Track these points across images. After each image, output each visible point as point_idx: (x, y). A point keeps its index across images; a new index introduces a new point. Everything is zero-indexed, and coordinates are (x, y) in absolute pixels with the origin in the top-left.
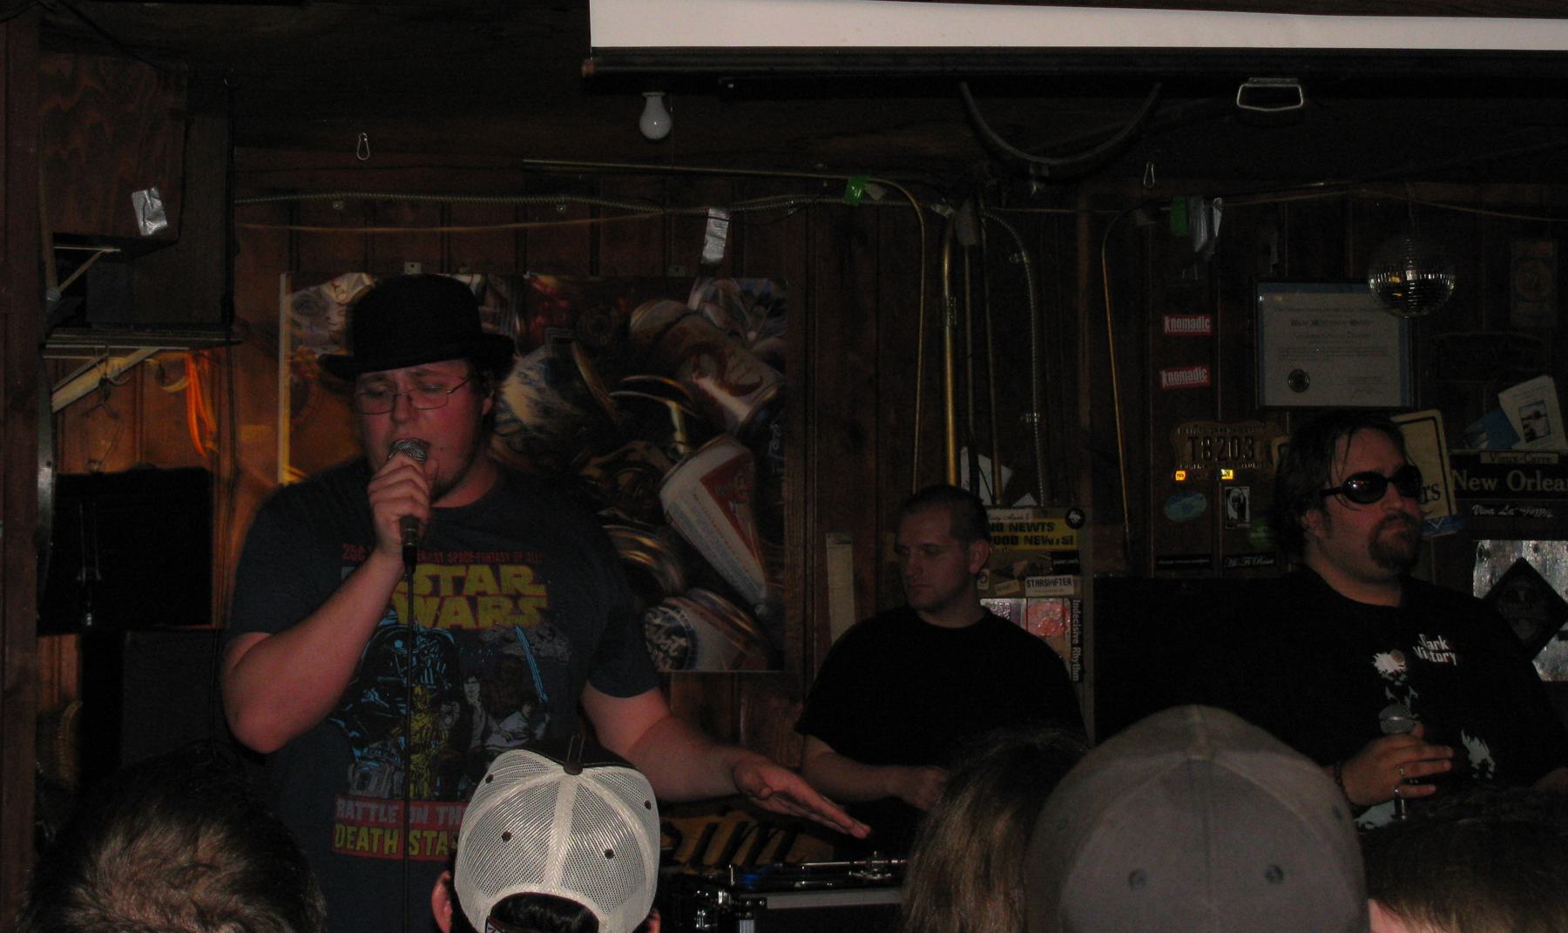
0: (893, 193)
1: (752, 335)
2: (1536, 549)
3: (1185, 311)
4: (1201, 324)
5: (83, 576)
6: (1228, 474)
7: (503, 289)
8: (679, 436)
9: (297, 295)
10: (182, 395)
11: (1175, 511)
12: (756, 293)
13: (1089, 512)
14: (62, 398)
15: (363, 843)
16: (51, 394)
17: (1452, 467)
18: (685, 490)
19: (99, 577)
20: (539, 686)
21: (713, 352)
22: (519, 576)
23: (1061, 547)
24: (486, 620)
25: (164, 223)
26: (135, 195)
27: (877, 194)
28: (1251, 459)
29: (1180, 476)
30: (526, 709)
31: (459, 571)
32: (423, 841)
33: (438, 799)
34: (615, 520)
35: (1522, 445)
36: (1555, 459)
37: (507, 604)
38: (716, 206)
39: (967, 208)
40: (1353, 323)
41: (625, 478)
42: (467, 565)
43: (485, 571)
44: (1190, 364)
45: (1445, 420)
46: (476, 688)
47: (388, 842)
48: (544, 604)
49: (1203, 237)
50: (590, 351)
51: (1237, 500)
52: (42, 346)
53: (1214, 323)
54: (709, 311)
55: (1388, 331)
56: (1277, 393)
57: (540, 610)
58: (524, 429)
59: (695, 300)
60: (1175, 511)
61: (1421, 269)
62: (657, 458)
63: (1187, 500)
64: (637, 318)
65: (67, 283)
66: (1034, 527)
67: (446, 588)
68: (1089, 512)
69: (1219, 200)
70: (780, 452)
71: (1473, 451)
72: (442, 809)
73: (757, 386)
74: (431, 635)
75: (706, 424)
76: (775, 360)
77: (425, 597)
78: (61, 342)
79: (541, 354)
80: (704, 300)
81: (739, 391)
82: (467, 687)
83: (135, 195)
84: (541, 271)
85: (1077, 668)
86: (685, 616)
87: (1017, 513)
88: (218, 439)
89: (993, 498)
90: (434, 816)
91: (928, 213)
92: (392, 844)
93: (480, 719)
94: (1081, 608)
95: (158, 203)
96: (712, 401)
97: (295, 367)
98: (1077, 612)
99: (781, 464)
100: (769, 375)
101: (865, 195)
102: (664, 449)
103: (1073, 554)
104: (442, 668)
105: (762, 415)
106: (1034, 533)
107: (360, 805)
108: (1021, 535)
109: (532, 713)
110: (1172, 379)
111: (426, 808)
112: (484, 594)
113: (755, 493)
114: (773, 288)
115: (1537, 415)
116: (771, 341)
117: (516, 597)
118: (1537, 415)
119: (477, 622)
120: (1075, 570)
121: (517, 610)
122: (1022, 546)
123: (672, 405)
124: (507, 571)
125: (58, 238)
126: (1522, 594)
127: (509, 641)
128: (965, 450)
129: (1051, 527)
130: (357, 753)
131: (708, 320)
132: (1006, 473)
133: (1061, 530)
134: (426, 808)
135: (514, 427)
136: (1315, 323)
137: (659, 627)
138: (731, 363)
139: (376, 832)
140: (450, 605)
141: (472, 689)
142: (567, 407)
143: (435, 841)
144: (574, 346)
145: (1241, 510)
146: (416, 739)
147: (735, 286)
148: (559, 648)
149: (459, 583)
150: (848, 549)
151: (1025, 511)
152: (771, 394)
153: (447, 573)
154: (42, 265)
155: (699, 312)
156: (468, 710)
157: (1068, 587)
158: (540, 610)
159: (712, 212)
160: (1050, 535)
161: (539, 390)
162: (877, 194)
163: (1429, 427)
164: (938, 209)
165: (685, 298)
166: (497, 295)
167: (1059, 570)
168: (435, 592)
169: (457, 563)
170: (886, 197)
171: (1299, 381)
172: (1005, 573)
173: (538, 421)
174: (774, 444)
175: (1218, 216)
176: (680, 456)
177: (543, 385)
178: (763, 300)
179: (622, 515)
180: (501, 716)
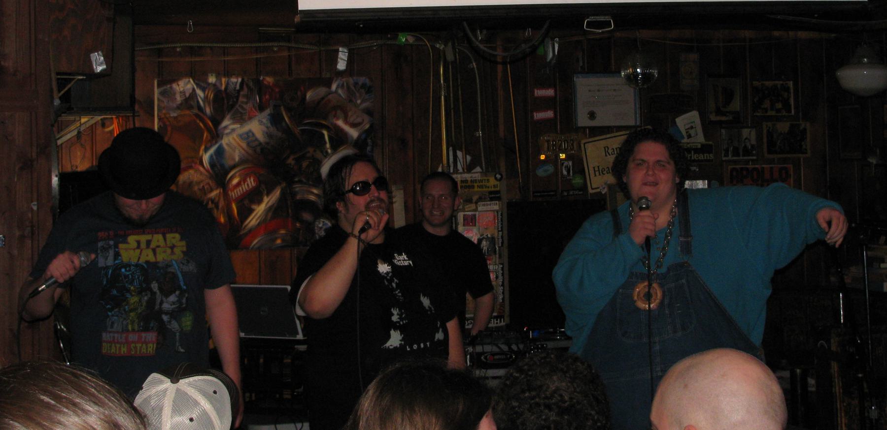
0: (418, 39)
1: (359, 102)
3: (543, 85)
4: (550, 92)
6: (563, 156)
7: (251, 84)
8: (328, 145)
9: (162, 89)
11: (541, 172)
12: (360, 83)
13: (504, 174)
15: (113, 350)
20: (182, 283)
21: (342, 109)
22: (174, 238)
23: (493, 189)
24: (160, 258)
25: (105, 67)
27: (411, 40)
28: (572, 150)
29: (543, 157)
30: (177, 293)
31: (149, 237)
32: (136, 348)
33: (142, 331)
34: (300, 182)
35: (685, 140)
36: (699, 146)
37: (169, 251)
38: (343, 46)
40: (615, 90)
41: (305, 164)
43: (160, 237)
44: (546, 109)
48: (185, 249)
49: (551, 55)
50: (289, 110)
51: (566, 167)
53: (556, 91)
54: (340, 91)
55: (629, 94)
56: (583, 120)
57: (183, 252)
58: (260, 144)
59: (334, 87)
60: (541, 172)
61: (642, 68)
62: (319, 155)
63: (546, 168)
64: (309, 95)
66: (481, 181)
67: (143, 245)
68: (504, 174)
70: (372, 151)
72: (143, 335)
74: (137, 265)
76: (369, 112)
79: (268, 111)
80: (337, 88)
81: (354, 125)
82: (152, 286)
85: (500, 241)
87: (474, 175)
91: (433, 47)
92: (124, 350)
95: (102, 58)
96: (342, 130)
97: (160, 119)
98: (500, 217)
100: (367, 118)
101: (406, 40)
102: (322, 152)
103: (498, 192)
105: (363, 136)
107: (112, 335)
108: (476, 185)
109: (180, 294)
110: (539, 116)
112: (158, 247)
114: (367, 81)
115: (692, 128)
116: (366, 105)
117: (173, 247)
118: (692, 128)
120: (499, 199)
121: (173, 253)
122: (476, 189)
124: (169, 236)
125: (58, 74)
127: (170, 266)
128: (451, 148)
130: (110, 314)
131: (340, 95)
132: (469, 158)
133: (492, 181)
135: (257, 143)
137: (321, 228)
138: (350, 114)
139: (118, 346)
141: (155, 286)
142: (280, 134)
145: (568, 172)
147: (351, 81)
148: (191, 267)
149: (148, 243)
150: (402, 192)
151: (476, 174)
152: (367, 126)
153: (143, 238)
155: (336, 92)
157: (495, 206)
158: (183, 252)
159: (340, 49)
161: (267, 127)
162: (411, 40)
164: (438, 46)
165: (329, 87)
166: (247, 85)
167: (492, 199)
168: (139, 247)
171: (592, 115)
173: (267, 140)
174: (369, 148)
177: (269, 125)
178: (364, 86)
180: (167, 296)
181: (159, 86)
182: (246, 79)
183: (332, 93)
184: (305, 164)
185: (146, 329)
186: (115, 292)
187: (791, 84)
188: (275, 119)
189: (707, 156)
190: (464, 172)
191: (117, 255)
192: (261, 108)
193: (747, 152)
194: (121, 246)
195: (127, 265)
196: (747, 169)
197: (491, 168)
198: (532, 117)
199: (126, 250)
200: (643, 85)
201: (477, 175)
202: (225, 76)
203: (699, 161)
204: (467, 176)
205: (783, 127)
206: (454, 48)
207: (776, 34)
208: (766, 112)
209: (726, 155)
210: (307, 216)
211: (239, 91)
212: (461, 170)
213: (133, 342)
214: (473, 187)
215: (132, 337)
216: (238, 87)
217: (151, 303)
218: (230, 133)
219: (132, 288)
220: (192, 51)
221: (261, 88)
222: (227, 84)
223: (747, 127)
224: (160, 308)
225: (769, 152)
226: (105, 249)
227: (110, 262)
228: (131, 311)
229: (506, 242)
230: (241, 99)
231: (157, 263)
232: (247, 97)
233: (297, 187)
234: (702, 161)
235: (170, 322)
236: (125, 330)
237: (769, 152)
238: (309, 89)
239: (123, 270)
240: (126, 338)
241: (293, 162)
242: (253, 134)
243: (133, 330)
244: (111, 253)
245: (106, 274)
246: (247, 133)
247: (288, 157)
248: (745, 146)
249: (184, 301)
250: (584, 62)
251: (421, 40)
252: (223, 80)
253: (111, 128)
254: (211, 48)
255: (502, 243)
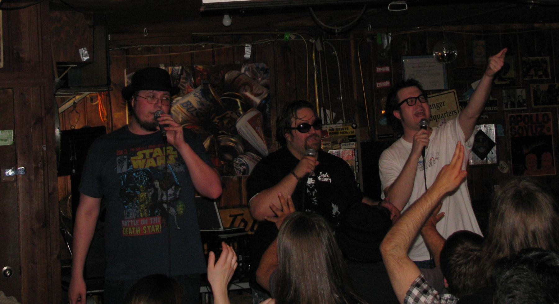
0: (297, 37)
1: (260, 79)
2: (485, 127)
3: (382, 65)
4: (387, 69)
5: (72, 159)
7: (188, 70)
8: (240, 109)
10: (97, 105)
12: (260, 67)
13: (358, 124)
14: (61, 109)
15: (130, 232)
16: (58, 108)
17: (460, 105)
18: (243, 124)
19: (76, 159)
20: (176, 180)
21: (249, 85)
23: (351, 134)
24: (159, 164)
26: (80, 50)
27: (293, 37)
30: (173, 187)
31: (151, 151)
32: (147, 229)
33: (150, 216)
34: (223, 134)
38: (247, 43)
39: (319, 40)
41: (225, 122)
42: (154, 148)
43: (158, 150)
44: (384, 80)
45: (457, 92)
46: (158, 183)
47: (137, 231)
49: (386, 44)
50: (214, 86)
52: (55, 95)
55: (440, 68)
58: (196, 109)
59: (243, 70)
61: (447, 50)
62: (234, 116)
64: (226, 76)
65: (61, 77)
67: (148, 156)
68: (358, 124)
69: (390, 34)
70: (270, 112)
71: (465, 100)
72: (151, 219)
73: (261, 94)
74: (144, 170)
75: (248, 105)
76: (266, 86)
77: (141, 160)
78: (60, 93)
79: (200, 88)
80: (245, 70)
81: (257, 95)
82: (155, 183)
83: (80, 50)
84: (199, 65)
85: (357, 168)
86: (245, 160)
87: (338, 125)
88: (107, 117)
89: (331, 121)
90: (149, 221)
91: (308, 42)
92: (138, 231)
93: (160, 192)
94: (357, 151)
95: (86, 52)
96: (249, 98)
98: (356, 152)
99: (270, 115)
100: (265, 90)
101: (290, 38)
102: (236, 113)
103: (355, 136)
104: (147, 179)
105: (264, 102)
106: (342, 131)
107: (128, 221)
108: (339, 132)
109: (175, 188)
110: (379, 85)
111: (147, 220)
112: (158, 156)
113: (262, 123)
119: (157, 164)
120: (355, 141)
122: (340, 135)
123: (238, 100)
125: (58, 63)
126: (481, 140)
129: (348, 129)
130: (126, 207)
132: (334, 114)
133: (350, 129)
134: (147, 220)
135: (193, 109)
136: (419, 67)
137: (238, 164)
138: (254, 88)
139: (134, 229)
140: (149, 161)
141: (157, 184)
142: (208, 103)
143: (151, 228)
144: (209, 85)
146: (142, 200)
147: (254, 66)
149: (151, 155)
151: (340, 125)
152: (266, 96)
153: (147, 152)
154: (53, 72)
155: (244, 73)
156: (156, 190)
159: (246, 45)
160: (347, 131)
161: (200, 98)
162: (293, 37)
163: (452, 94)
164: (311, 41)
165: (240, 70)
166: (186, 72)
167: (350, 141)
169: (151, 148)
170: (296, 38)
172: (335, 143)
173: (200, 107)
174: (267, 110)
175: (390, 38)
176: (241, 115)
177: (201, 97)
178: (263, 69)
179: (225, 133)
180: (166, 190)
181: (127, 74)
182: (184, 67)
183: (242, 74)
184: (225, 122)
185: (153, 215)
186: (129, 190)
187: (547, 58)
188: (205, 93)
189: (493, 108)
190: (331, 124)
191: (130, 164)
192: (195, 86)
193: (520, 104)
194: (132, 158)
195: (137, 171)
196: (521, 116)
197: (349, 120)
198: (376, 86)
199: (136, 160)
200: (448, 60)
201: (339, 125)
202: (170, 66)
203: (488, 111)
204: (334, 126)
205: (544, 87)
206: (321, 41)
207: (536, 25)
208: (532, 78)
209: (507, 107)
210: (228, 156)
211: (180, 75)
212: (329, 122)
213: (144, 225)
214: (338, 133)
215: (143, 222)
216: (179, 73)
217: (155, 195)
218: (176, 103)
219: (141, 186)
220: (149, 50)
221: (195, 73)
222: (172, 71)
223: (519, 88)
224: (161, 199)
225: (535, 104)
226: (121, 162)
227: (125, 169)
228: (141, 203)
229: (361, 170)
230: (182, 80)
231: (157, 167)
232: (186, 79)
233: (221, 138)
234: (490, 111)
235: (168, 209)
236: (138, 217)
237: (535, 104)
238: (227, 72)
239: (134, 174)
240: (139, 223)
241: (217, 121)
242: (191, 104)
243: (144, 217)
244: (125, 164)
245: (123, 178)
246: (186, 103)
247: (214, 118)
248: (519, 101)
249: (178, 193)
250: (408, 49)
251: (300, 38)
252: (170, 68)
253: (96, 103)
254: (161, 48)
255: (358, 170)
